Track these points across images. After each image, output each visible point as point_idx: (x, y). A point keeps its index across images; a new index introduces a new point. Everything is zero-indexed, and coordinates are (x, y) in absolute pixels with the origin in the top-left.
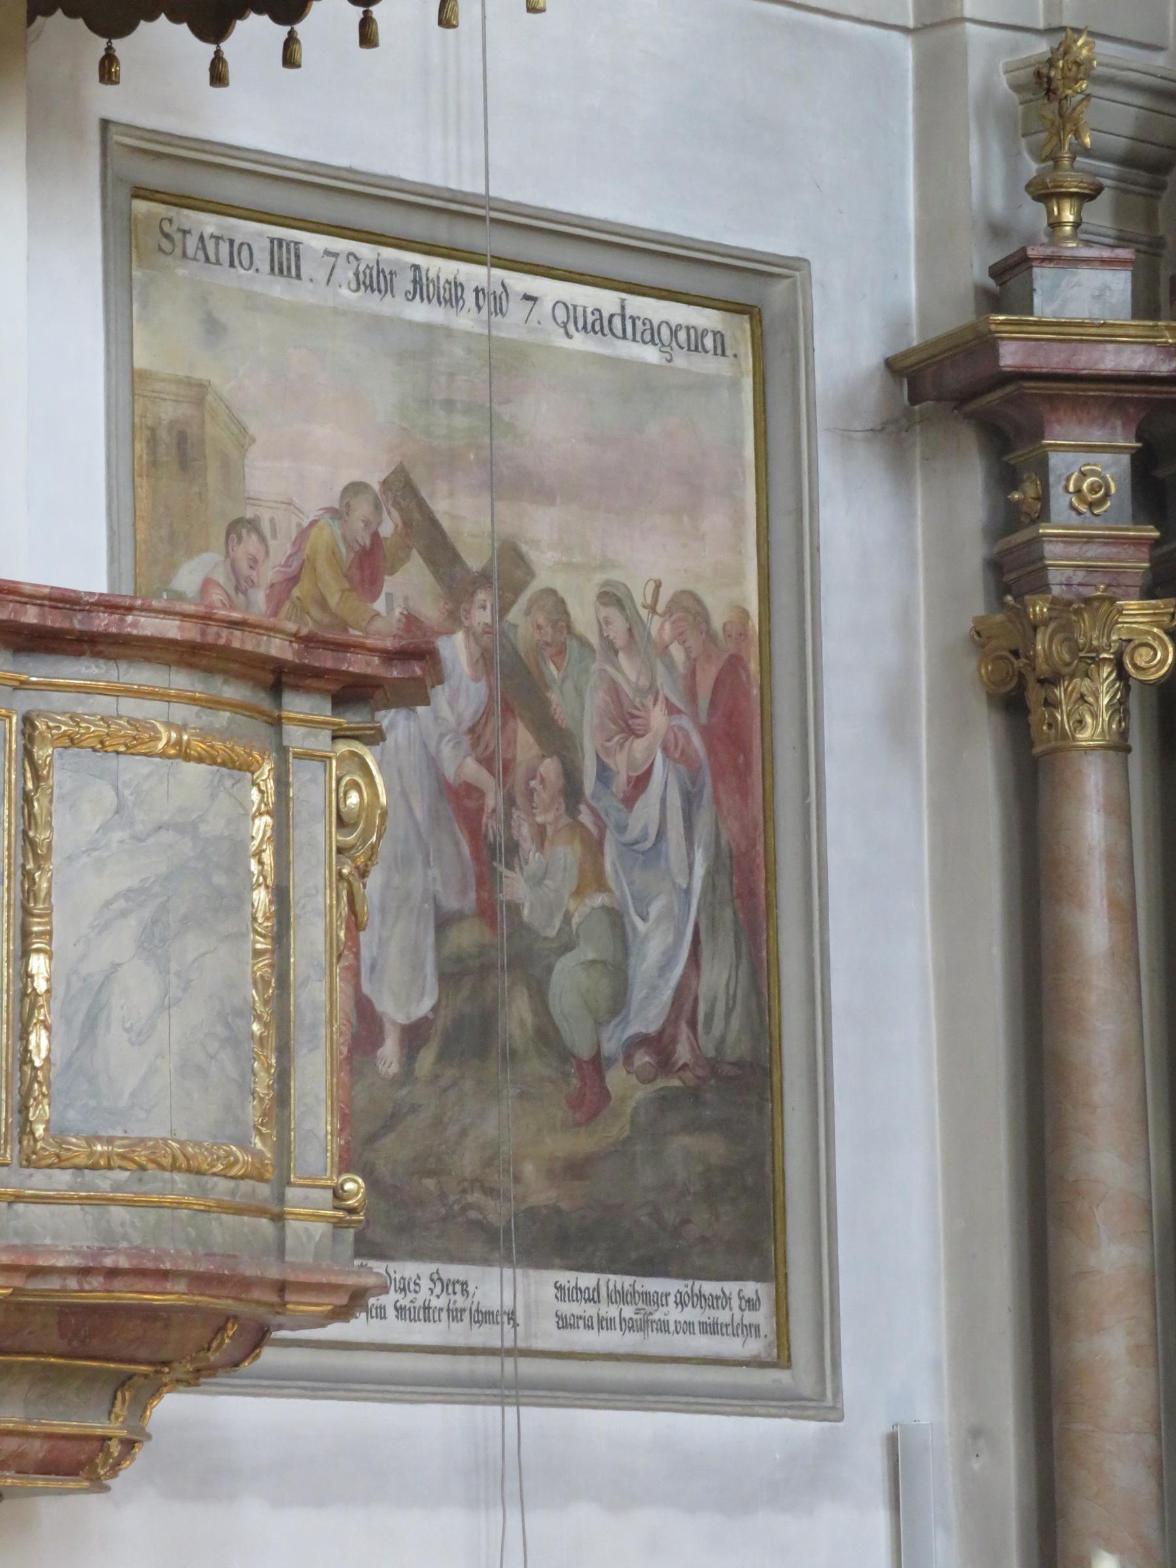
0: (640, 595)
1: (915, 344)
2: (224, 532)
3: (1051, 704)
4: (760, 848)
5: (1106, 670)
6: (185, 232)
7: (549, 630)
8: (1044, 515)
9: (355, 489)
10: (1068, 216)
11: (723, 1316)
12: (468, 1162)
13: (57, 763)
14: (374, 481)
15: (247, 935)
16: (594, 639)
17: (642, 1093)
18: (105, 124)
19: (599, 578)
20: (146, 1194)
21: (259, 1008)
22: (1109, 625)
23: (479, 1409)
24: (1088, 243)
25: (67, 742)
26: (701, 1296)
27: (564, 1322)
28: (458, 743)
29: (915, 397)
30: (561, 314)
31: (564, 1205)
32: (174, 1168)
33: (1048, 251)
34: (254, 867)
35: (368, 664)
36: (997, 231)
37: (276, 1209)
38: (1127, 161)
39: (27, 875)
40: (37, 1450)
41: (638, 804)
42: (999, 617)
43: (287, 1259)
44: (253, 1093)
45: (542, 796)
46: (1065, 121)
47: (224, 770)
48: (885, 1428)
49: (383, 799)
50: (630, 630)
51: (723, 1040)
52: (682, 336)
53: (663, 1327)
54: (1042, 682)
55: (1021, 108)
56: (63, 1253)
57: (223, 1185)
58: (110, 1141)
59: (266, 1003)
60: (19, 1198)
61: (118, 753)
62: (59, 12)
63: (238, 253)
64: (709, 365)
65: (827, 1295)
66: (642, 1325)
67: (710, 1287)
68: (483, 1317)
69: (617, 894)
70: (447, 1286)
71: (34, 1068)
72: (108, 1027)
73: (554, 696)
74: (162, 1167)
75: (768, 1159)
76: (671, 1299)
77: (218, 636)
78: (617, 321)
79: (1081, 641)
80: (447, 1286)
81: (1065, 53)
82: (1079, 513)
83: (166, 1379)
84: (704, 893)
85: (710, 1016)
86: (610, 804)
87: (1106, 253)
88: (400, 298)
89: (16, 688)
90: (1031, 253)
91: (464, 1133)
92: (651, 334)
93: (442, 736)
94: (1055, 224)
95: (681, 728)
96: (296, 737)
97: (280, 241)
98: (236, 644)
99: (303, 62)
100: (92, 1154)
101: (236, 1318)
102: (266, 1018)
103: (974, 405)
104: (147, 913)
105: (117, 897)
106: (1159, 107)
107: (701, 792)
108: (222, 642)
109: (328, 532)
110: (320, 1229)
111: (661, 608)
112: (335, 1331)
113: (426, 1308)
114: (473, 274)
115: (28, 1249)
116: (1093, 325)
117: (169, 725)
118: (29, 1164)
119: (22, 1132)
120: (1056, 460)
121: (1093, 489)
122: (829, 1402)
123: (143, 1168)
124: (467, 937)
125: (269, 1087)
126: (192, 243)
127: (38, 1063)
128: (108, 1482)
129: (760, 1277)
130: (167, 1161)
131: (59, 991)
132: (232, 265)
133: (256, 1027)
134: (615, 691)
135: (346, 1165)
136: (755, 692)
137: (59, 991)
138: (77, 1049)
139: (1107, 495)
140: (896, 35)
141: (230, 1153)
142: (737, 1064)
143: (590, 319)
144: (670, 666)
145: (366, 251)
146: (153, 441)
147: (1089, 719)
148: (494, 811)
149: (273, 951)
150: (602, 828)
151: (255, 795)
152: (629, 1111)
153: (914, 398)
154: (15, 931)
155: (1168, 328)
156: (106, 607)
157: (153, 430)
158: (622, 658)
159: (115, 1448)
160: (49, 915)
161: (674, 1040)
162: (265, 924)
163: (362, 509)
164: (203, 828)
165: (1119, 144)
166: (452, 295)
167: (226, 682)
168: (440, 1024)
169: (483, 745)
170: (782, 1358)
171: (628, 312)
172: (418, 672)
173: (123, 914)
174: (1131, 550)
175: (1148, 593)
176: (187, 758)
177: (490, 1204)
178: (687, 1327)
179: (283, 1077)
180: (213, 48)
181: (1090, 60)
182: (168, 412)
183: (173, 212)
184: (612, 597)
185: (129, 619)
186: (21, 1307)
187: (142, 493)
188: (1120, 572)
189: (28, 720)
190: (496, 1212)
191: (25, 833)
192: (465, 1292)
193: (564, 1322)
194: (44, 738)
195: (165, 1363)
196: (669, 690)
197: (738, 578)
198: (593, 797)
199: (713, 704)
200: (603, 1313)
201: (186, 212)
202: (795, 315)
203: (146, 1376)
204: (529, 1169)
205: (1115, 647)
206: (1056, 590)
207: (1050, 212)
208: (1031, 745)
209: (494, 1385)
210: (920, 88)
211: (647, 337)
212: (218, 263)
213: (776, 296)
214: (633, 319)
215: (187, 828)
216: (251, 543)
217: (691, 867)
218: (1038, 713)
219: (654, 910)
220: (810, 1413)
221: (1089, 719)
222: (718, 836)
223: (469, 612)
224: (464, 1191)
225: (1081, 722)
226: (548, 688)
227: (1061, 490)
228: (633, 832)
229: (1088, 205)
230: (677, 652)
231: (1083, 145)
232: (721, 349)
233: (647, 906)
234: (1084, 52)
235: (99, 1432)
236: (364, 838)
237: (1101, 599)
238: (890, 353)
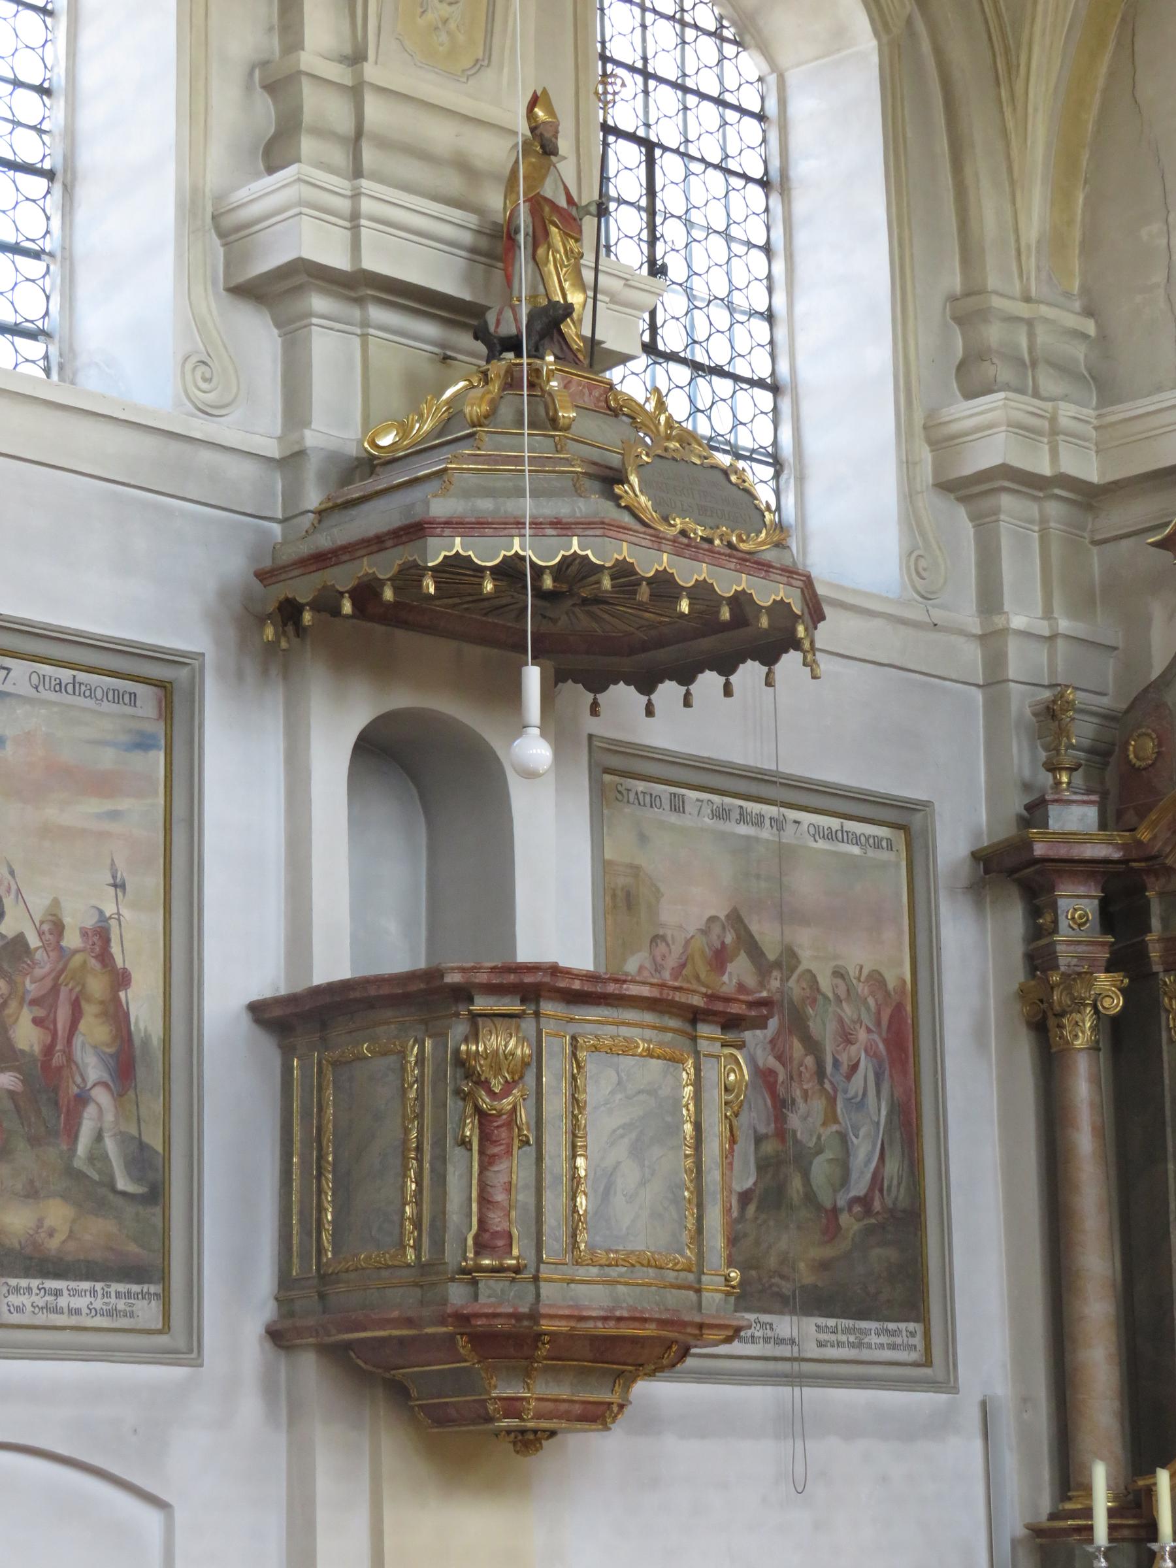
0: (853, 972)
1: (985, 845)
2: (649, 940)
3: (1061, 1026)
4: (913, 1102)
5: (1088, 1009)
6: (629, 790)
7: (808, 990)
8: (1055, 930)
9: (712, 919)
10: (1065, 779)
11: (898, 1340)
12: (772, 1262)
13: (588, 1060)
14: (722, 915)
15: (681, 1147)
16: (830, 995)
17: (857, 1226)
18: (590, 736)
19: (833, 963)
20: (635, 1279)
21: (688, 1183)
22: (1090, 986)
23: (780, 1388)
24: (1075, 793)
25: (594, 1049)
26: (887, 1330)
27: (820, 1344)
28: (765, 1049)
29: (987, 871)
30: (812, 830)
31: (820, 1284)
32: (649, 1265)
33: (1056, 797)
34: (685, 1112)
35: (740, 1008)
36: (1027, 787)
37: (697, 1286)
38: (1091, 751)
39: (575, 1117)
40: (577, 1409)
41: (854, 1079)
42: (1033, 983)
43: (703, 1311)
44: (686, 1227)
45: (806, 1075)
46: (1062, 731)
47: (670, 1063)
48: (980, 1398)
49: (747, 1077)
50: (848, 990)
51: (896, 1198)
52: (871, 841)
53: (869, 1346)
54: (1055, 1015)
56: (594, 1309)
57: (672, 1274)
58: (616, 1252)
59: (691, 1181)
60: (573, 1281)
62: (570, 681)
63: (654, 801)
64: (884, 856)
66: (858, 1345)
67: (891, 1326)
68: (780, 1341)
69: (844, 1125)
70: (763, 1325)
71: (579, 1215)
72: (615, 1193)
73: (811, 1024)
74: (642, 1265)
75: (919, 1259)
76: (873, 1332)
77: (668, 994)
78: (839, 834)
79: (1076, 994)
80: (763, 1325)
81: (1061, 697)
82: (1073, 929)
83: (641, 1373)
84: (885, 1127)
85: (890, 1187)
86: (839, 1079)
87: (1085, 798)
88: (733, 822)
89: (568, 1022)
90: (1047, 797)
91: (770, 1247)
92: (856, 840)
93: (757, 1045)
94: (1058, 783)
95: (874, 1040)
96: (704, 1046)
97: (675, 794)
98: (677, 999)
99: (602, 714)
100: (609, 1258)
101: (677, 1342)
102: (692, 1189)
103: (1016, 876)
104: (633, 1135)
105: (618, 1128)
106: (1107, 724)
107: (884, 1073)
108: (670, 998)
109: (699, 942)
110: (718, 1297)
111: (863, 979)
112: (723, 1349)
113: (753, 1337)
114: (771, 811)
115: (577, 1307)
116: (1080, 834)
117: (643, 1040)
118: (577, 1264)
119: (574, 1248)
120: (1062, 903)
121: (1081, 917)
123: (633, 1265)
124: (769, 1147)
125: (693, 1224)
126: (632, 796)
127: (581, 1212)
128: (611, 1426)
129: (916, 1320)
130: (645, 1262)
131: (591, 1176)
132: (651, 806)
133: (686, 1194)
134: (841, 1021)
135: (730, 1263)
136: (910, 1021)
137: (591, 1176)
139: (1088, 920)
140: (973, 688)
141: (675, 1258)
142: (904, 1211)
143: (826, 833)
144: (868, 1009)
145: (716, 799)
146: (614, 896)
147: (1080, 1034)
148: (783, 1082)
149: (694, 1155)
150: (835, 1090)
151: (684, 1075)
152: (851, 1235)
153: (987, 872)
154: (569, 1145)
155: (1119, 835)
157: (614, 890)
158: (844, 1004)
159: (615, 1409)
160: (585, 1137)
161: (872, 1200)
162: (690, 1141)
163: (716, 930)
164: (660, 1092)
165: (1086, 743)
166: (758, 821)
167: (670, 1018)
168: (757, 1192)
169: (776, 1049)
170: (928, 1362)
171: (845, 829)
172: (765, 1012)
173: (622, 1136)
174: (1100, 948)
175: (1107, 971)
176: (652, 1056)
177: (783, 1283)
178: (881, 1346)
179: (700, 1219)
180: (647, 697)
181: (1074, 700)
182: (621, 881)
183: (622, 780)
184: (839, 974)
185: (625, 986)
186: (572, 1336)
187: (609, 922)
188: (1095, 959)
189: (574, 1038)
190: (786, 1288)
191: (573, 1095)
192: (771, 1328)
193: (820, 1344)
194: (582, 1047)
195: (641, 1365)
196: (868, 1020)
197: (900, 964)
198: (831, 1075)
199: (889, 1027)
200: (839, 1339)
201: (629, 780)
202: (927, 831)
203: (631, 1372)
204: (802, 1265)
205: (1093, 997)
206: (1062, 969)
207: (1055, 777)
208: (1050, 1048)
209: (786, 1376)
211: (854, 842)
212: (645, 805)
213: (917, 820)
214: (80, 684)
215: (652, 1092)
216: (662, 947)
217: (879, 1110)
218: (1054, 1032)
219: (862, 1133)
220: (943, 1390)
221: (1080, 1034)
222: (892, 1096)
223: (769, 982)
224: (770, 1277)
225: (1076, 1036)
226: (808, 1020)
227: (1064, 917)
228: (851, 1093)
229: (1075, 773)
230: (871, 1001)
231: (1072, 744)
232: (890, 847)
233: (859, 1130)
234: (1071, 696)
235: (608, 1400)
236: (738, 1096)
238: (974, 849)
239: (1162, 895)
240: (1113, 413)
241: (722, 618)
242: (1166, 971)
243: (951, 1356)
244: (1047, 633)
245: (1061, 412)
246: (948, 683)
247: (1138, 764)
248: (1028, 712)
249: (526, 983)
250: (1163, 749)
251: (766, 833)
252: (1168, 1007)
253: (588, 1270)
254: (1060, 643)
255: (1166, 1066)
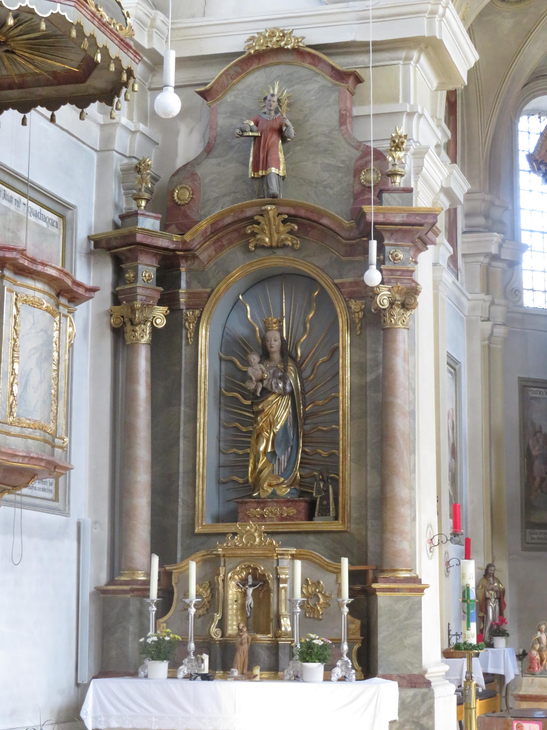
11: (46, 487)
29: (96, 246)
55: (122, 176)
58: (30, 420)
61: (34, 307)
65: (68, 484)
78: (39, 214)
92: (45, 219)
94: (139, 206)
120: (140, 267)
122: (67, 512)
138: (22, 392)
140: (93, 151)
156: (42, 264)
162: (55, 362)
185: (46, 268)
210: (98, 166)
213: (69, 214)
225: (142, 337)
237: (151, 305)
239: (188, 271)
240: (180, 23)
241: (111, 70)
242: (187, 309)
243: (67, 497)
244: (133, 130)
245: (158, 17)
246: (85, 146)
247: (179, 202)
248: (119, 168)
249: (6, 257)
250: (194, 196)
251: (13, 207)
252: (187, 327)
253: (15, 429)
254: (138, 135)
255: (183, 357)
